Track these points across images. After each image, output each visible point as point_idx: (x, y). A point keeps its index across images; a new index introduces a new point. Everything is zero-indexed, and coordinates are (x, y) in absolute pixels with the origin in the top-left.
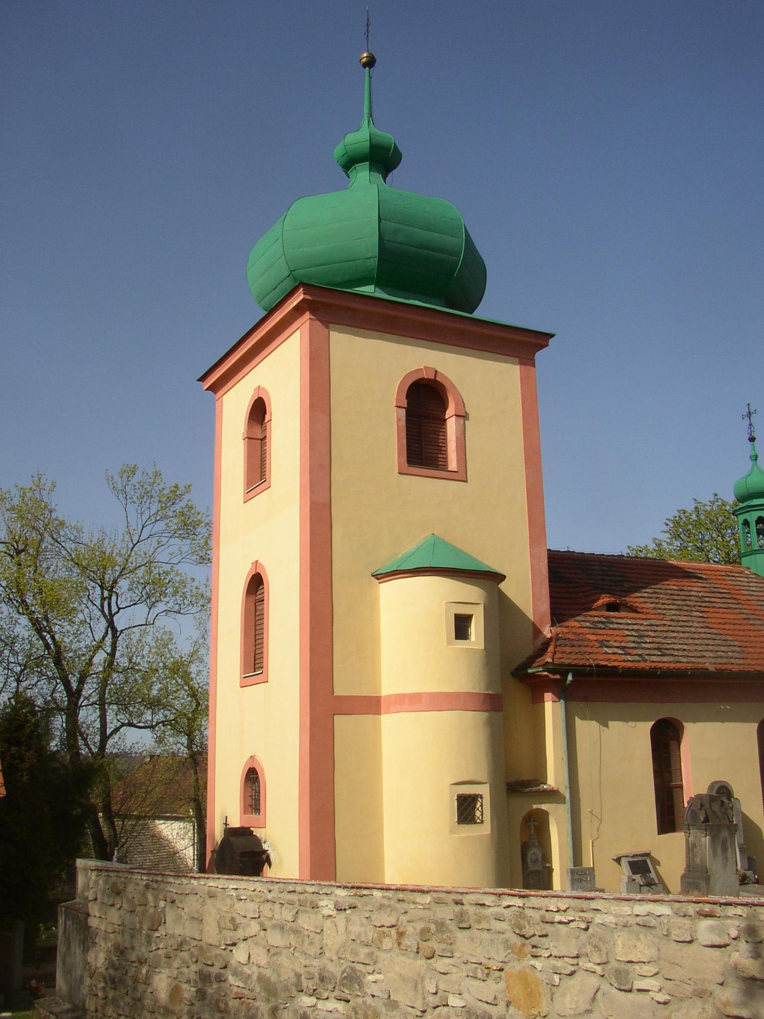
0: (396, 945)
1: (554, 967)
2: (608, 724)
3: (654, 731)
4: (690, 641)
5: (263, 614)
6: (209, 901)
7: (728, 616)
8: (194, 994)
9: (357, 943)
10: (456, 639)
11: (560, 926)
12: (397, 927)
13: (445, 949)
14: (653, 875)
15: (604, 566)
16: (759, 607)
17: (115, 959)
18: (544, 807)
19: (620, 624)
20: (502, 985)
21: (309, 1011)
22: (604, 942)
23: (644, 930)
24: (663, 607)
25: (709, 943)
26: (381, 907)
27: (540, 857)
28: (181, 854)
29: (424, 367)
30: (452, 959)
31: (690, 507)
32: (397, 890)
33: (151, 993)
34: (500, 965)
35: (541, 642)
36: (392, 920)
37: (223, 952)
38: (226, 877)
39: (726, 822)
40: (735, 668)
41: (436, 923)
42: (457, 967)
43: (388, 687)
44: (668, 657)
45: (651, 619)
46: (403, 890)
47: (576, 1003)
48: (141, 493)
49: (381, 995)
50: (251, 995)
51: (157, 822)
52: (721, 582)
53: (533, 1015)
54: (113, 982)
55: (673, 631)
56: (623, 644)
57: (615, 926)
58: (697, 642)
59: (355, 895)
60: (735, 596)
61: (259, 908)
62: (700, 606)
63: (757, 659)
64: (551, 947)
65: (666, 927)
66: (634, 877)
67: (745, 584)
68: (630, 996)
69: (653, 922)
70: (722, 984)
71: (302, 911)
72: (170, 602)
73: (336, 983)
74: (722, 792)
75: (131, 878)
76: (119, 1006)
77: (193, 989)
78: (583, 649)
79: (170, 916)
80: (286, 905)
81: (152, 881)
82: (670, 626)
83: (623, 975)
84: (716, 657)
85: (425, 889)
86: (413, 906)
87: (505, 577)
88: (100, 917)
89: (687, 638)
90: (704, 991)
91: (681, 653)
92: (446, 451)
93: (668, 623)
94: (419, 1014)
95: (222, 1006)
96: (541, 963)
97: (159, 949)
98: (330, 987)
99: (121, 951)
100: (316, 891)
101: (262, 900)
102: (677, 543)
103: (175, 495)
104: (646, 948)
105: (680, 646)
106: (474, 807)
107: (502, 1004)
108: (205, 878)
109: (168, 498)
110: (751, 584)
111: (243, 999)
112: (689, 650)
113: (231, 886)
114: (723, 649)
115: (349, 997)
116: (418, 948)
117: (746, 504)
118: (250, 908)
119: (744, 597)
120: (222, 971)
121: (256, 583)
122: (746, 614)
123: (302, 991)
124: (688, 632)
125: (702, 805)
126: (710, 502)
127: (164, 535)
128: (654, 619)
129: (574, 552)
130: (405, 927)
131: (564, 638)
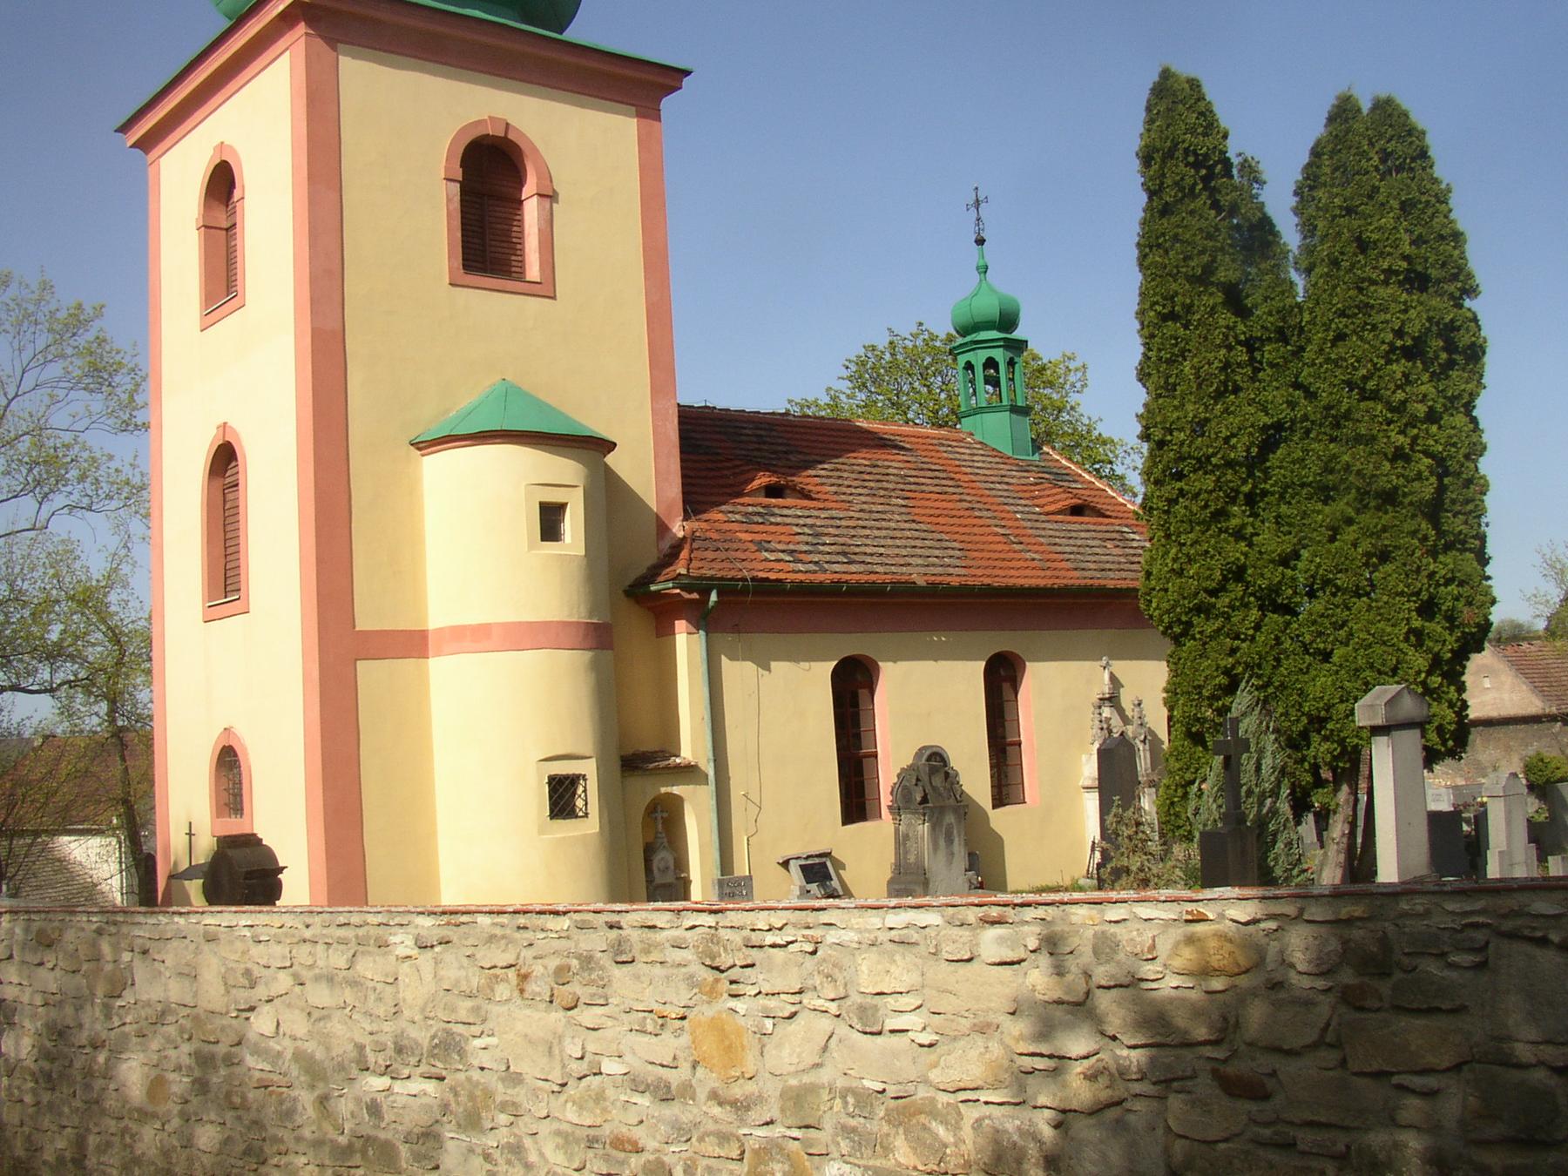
0: (516, 993)
1: (765, 1008)
2: (769, 665)
3: (837, 675)
4: (890, 542)
5: (238, 506)
6: (206, 947)
7: (945, 505)
8: (189, 1086)
9: (454, 994)
10: (542, 540)
11: (771, 950)
12: (518, 967)
13: (595, 994)
14: (835, 883)
15: (761, 429)
16: (987, 492)
17: (49, 1044)
18: (676, 790)
19: (786, 516)
20: (685, 1039)
21: (380, 1097)
22: (841, 969)
23: (901, 948)
24: (849, 491)
25: (998, 960)
26: (492, 938)
27: (671, 864)
28: (104, 887)
29: (490, 117)
30: (606, 1008)
31: (882, 342)
32: (515, 912)
33: (117, 1090)
34: (682, 1012)
35: (668, 545)
36: (509, 958)
37: (234, 1022)
38: (234, 909)
39: (952, 801)
40: (955, 582)
41: (579, 957)
42: (615, 1019)
43: (437, 617)
44: (857, 566)
45: (831, 509)
46: (525, 912)
47: (799, 1056)
48: (18, 317)
49: (494, 1066)
50: (284, 1081)
51: (66, 839)
52: (933, 454)
53: (733, 1077)
54: (48, 1080)
55: (864, 527)
56: (791, 547)
57: (856, 946)
58: (898, 542)
59: (448, 924)
60: (952, 475)
61: (290, 952)
62: (902, 490)
63: (986, 568)
64: (760, 981)
65: (934, 942)
66: (809, 887)
67: (967, 457)
68: (879, 1039)
69: (915, 937)
70: (1013, 1014)
71: (362, 952)
72: (74, 492)
73: (422, 1054)
74: (935, 762)
75: (70, 921)
76: (60, 1114)
77: (185, 1080)
78: (732, 554)
79: (140, 971)
80: (335, 945)
81: (107, 923)
82: (859, 519)
83: (870, 1012)
84: (927, 566)
85: (561, 908)
86: (542, 935)
87: (615, 445)
88: (20, 984)
89: (885, 537)
90: (989, 1025)
91: (876, 559)
92: (522, 250)
93: (857, 515)
94: (556, 1088)
95: (237, 1100)
96: (745, 1003)
97: (124, 1024)
98: (413, 1061)
99: (59, 1033)
100: (384, 922)
101: (295, 940)
102: (861, 396)
103: (77, 321)
104: (905, 971)
105: (875, 550)
106: (574, 793)
107: (685, 1068)
108: (197, 912)
109: (65, 325)
110: (975, 458)
111: (270, 1089)
112: (888, 555)
113: (243, 923)
114: (937, 553)
115: (444, 1073)
116: (552, 995)
117: (968, 338)
118: (277, 954)
119: (966, 478)
120: (233, 1049)
121: (225, 458)
122: (970, 502)
123: (367, 1069)
124: (886, 529)
125: (918, 780)
126: (911, 335)
127: (61, 385)
128: (836, 509)
129: (714, 408)
130: (530, 966)
131: (703, 537)
